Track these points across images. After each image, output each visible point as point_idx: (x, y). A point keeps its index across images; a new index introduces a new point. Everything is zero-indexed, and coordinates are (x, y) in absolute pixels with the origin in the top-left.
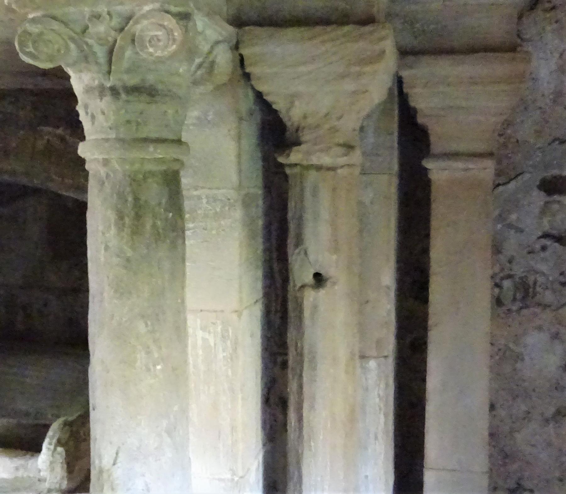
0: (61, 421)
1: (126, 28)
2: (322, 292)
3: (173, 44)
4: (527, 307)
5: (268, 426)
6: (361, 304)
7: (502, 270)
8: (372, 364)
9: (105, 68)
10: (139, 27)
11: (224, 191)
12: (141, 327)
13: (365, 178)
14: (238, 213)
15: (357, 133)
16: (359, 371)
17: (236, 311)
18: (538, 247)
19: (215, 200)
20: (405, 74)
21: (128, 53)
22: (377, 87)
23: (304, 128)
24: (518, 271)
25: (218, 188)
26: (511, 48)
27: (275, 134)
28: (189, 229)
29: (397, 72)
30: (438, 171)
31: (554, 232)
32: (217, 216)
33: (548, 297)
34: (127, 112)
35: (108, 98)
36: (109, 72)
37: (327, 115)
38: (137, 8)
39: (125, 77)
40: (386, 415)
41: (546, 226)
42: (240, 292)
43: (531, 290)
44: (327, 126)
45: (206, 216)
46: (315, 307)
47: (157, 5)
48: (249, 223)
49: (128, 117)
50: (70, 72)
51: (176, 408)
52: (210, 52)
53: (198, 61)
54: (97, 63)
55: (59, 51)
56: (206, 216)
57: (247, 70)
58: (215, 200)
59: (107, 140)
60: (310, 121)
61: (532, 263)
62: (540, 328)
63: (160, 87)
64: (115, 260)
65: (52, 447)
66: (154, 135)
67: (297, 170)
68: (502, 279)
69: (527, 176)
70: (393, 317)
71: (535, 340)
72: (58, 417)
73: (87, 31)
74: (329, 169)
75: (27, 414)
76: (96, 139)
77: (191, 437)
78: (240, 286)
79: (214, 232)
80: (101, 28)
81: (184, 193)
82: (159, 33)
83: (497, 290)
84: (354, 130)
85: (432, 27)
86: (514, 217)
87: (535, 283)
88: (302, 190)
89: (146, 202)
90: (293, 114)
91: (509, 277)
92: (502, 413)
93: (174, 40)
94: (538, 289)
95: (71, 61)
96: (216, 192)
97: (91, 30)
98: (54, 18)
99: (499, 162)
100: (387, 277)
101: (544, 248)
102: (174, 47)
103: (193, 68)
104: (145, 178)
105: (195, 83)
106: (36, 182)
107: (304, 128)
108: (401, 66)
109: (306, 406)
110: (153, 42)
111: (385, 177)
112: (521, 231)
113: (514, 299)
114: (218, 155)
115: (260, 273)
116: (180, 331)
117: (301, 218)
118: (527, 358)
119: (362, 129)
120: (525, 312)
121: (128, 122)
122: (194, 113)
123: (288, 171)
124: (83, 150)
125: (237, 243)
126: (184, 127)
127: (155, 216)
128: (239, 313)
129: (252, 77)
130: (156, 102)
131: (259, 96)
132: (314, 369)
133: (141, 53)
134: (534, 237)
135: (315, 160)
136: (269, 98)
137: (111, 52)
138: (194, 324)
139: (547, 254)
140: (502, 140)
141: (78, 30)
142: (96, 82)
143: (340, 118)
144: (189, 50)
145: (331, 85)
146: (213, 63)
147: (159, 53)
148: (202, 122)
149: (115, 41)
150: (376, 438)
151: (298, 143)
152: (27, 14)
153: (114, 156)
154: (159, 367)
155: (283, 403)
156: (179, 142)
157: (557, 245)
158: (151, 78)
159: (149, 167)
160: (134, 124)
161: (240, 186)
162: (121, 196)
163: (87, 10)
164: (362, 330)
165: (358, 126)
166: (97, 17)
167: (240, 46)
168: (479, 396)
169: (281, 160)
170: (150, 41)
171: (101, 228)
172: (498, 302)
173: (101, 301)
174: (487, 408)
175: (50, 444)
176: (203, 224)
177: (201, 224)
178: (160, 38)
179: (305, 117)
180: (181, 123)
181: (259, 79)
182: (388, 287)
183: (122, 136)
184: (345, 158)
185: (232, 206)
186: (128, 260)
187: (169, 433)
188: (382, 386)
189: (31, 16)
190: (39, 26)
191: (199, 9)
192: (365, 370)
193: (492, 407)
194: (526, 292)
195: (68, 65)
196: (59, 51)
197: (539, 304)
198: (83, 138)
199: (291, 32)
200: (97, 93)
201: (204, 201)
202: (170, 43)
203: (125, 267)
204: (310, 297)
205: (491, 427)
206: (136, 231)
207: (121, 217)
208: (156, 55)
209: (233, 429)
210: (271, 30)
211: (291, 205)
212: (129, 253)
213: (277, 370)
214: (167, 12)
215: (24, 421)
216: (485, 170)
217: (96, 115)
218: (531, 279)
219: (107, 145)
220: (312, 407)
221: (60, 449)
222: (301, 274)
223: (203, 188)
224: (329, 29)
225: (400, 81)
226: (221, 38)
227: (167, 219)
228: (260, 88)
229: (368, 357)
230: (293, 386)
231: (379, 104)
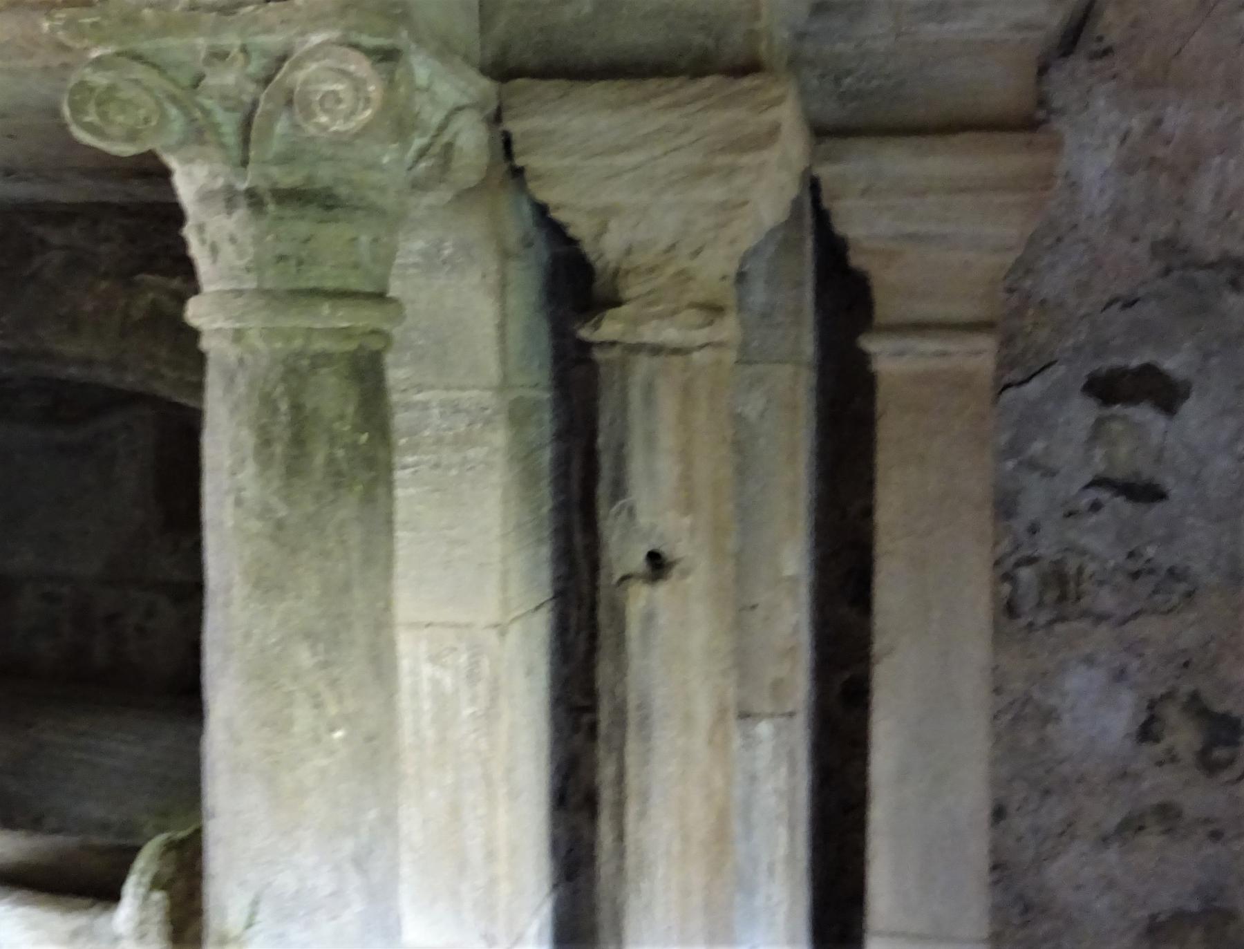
0: (161, 839)
1: (278, 77)
2: (662, 590)
3: (365, 108)
4: (1061, 619)
5: (563, 853)
6: (740, 612)
7: (1017, 547)
8: (764, 729)
9: (236, 153)
10: (301, 75)
11: (474, 393)
12: (304, 656)
13: (750, 370)
14: (499, 437)
15: (728, 283)
16: (737, 742)
17: (496, 626)
18: (1085, 502)
19: (457, 410)
20: (825, 172)
21: (281, 126)
22: (767, 194)
23: (627, 272)
24: (1047, 548)
25: (462, 388)
26: (1028, 122)
27: (573, 285)
28: (405, 467)
29: (810, 167)
30: (888, 357)
31: (1118, 474)
32: (461, 442)
33: (1106, 600)
34: (278, 239)
35: (242, 212)
36: (245, 163)
37: (673, 247)
38: (298, 40)
39: (275, 172)
40: (792, 828)
41: (1099, 464)
42: (504, 588)
43: (1072, 585)
44: (671, 270)
45: (439, 441)
46: (649, 618)
47: (334, 34)
48: (522, 457)
49: (282, 249)
50: (172, 162)
51: (372, 815)
52: (442, 128)
53: (418, 142)
54: (222, 146)
55: (146, 120)
56: (439, 441)
57: (519, 162)
58: (457, 410)
59: (239, 293)
60: (640, 259)
61: (1072, 535)
62: (1089, 661)
63: (343, 191)
64: (255, 525)
65: (142, 890)
66: (330, 284)
67: (615, 353)
68: (1018, 564)
69: (1059, 371)
70: (805, 638)
71: (1079, 682)
72: (161, 830)
73: (203, 83)
74: (677, 351)
75: (104, 827)
76: (218, 291)
77: (406, 870)
78: (505, 574)
79: (454, 472)
80: (227, 78)
81: (395, 397)
82: (339, 87)
83: (1006, 588)
84: (724, 278)
85: (875, 83)
86: (1038, 447)
87: (1080, 571)
88: (624, 391)
89: (316, 410)
90: (608, 248)
91: (1030, 561)
92: (1019, 823)
93: (368, 100)
94: (1086, 586)
95: (172, 140)
96: (454, 395)
97: (210, 81)
98: (138, 58)
99: (1007, 341)
100: (792, 559)
101: (1096, 507)
102: (368, 113)
103: (411, 154)
104: (314, 367)
105: (418, 186)
106: (130, 380)
107: (627, 272)
108: (815, 157)
109: (632, 809)
110: (327, 105)
111: (788, 369)
112: (1050, 473)
113: (1040, 605)
114: (460, 324)
115: (546, 551)
116: (382, 665)
117: (621, 445)
118: (1066, 718)
119: (741, 277)
120: (1060, 628)
121: (282, 258)
122: (413, 246)
123: (598, 355)
124: (196, 312)
125: (499, 492)
126: (394, 271)
127: (333, 440)
128: (501, 629)
129: (527, 175)
130: (336, 220)
131: (541, 211)
132: (647, 739)
133: (304, 125)
134: (1076, 488)
135: (648, 334)
136: (560, 216)
137: (247, 125)
138: (410, 650)
139: (1103, 516)
140: (1014, 300)
141: (185, 80)
142: (220, 182)
143: (697, 253)
144: (399, 122)
145: (681, 195)
146: (449, 146)
147: (339, 126)
148: (431, 262)
149: (255, 104)
150: (771, 870)
151: (618, 303)
152: (87, 49)
153: (254, 325)
154: (339, 734)
155: (591, 802)
156: (380, 297)
157: (1120, 500)
158: (325, 175)
159: (320, 345)
160: (293, 262)
161: (504, 385)
162: (268, 402)
163: (201, 43)
164: (742, 661)
165: (732, 269)
166: (219, 56)
167: (506, 115)
168: (971, 795)
169: (585, 333)
170: (321, 102)
171: (227, 463)
172: (1010, 609)
173: (227, 605)
174: (985, 814)
175: (139, 884)
176: (432, 458)
177: (425, 458)
178: (342, 96)
179: (629, 251)
180: (389, 260)
181: (538, 177)
182: (794, 580)
183: (268, 285)
184: (706, 331)
185: (488, 421)
186: (280, 525)
187: (360, 862)
188: (783, 771)
189: (95, 54)
190: (110, 74)
191: (419, 42)
192: (750, 742)
193: (999, 813)
194: (1062, 587)
195: (170, 149)
196: (146, 120)
197: (1085, 614)
198: (196, 291)
199: (599, 91)
200: (221, 204)
201: (436, 411)
202: (361, 105)
203: (273, 539)
204: (639, 598)
205: (994, 850)
206: (295, 467)
207: (265, 442)
208: (334, 128)
209: (491, 856)
210: (563, 83)
211: (604, 421)
212: (282, 511)
213: (579, 739)
214: (356, 46)
215: (97, 840)
216: (978, 356)
217: (216, 242)
218: (1072, 565)
219: (240, 301)
220: (642, 815)
221: (158, 896)
222: (624, 553)
223: (432, 387)
224: (674, 82)
225: (813, 186)
226: (465, 101)
227: (355, 446)
228: (543, 196)
229: (759, 715)
230: (607, 772)
231: (773, 231)
